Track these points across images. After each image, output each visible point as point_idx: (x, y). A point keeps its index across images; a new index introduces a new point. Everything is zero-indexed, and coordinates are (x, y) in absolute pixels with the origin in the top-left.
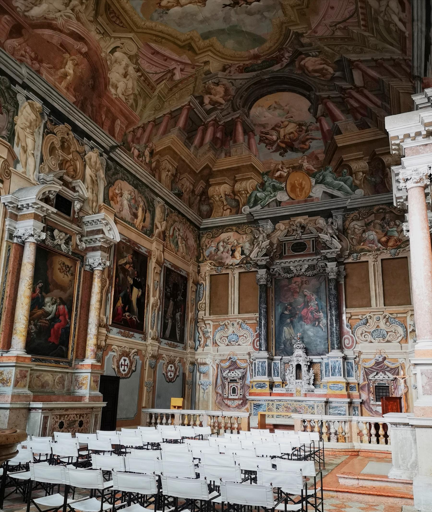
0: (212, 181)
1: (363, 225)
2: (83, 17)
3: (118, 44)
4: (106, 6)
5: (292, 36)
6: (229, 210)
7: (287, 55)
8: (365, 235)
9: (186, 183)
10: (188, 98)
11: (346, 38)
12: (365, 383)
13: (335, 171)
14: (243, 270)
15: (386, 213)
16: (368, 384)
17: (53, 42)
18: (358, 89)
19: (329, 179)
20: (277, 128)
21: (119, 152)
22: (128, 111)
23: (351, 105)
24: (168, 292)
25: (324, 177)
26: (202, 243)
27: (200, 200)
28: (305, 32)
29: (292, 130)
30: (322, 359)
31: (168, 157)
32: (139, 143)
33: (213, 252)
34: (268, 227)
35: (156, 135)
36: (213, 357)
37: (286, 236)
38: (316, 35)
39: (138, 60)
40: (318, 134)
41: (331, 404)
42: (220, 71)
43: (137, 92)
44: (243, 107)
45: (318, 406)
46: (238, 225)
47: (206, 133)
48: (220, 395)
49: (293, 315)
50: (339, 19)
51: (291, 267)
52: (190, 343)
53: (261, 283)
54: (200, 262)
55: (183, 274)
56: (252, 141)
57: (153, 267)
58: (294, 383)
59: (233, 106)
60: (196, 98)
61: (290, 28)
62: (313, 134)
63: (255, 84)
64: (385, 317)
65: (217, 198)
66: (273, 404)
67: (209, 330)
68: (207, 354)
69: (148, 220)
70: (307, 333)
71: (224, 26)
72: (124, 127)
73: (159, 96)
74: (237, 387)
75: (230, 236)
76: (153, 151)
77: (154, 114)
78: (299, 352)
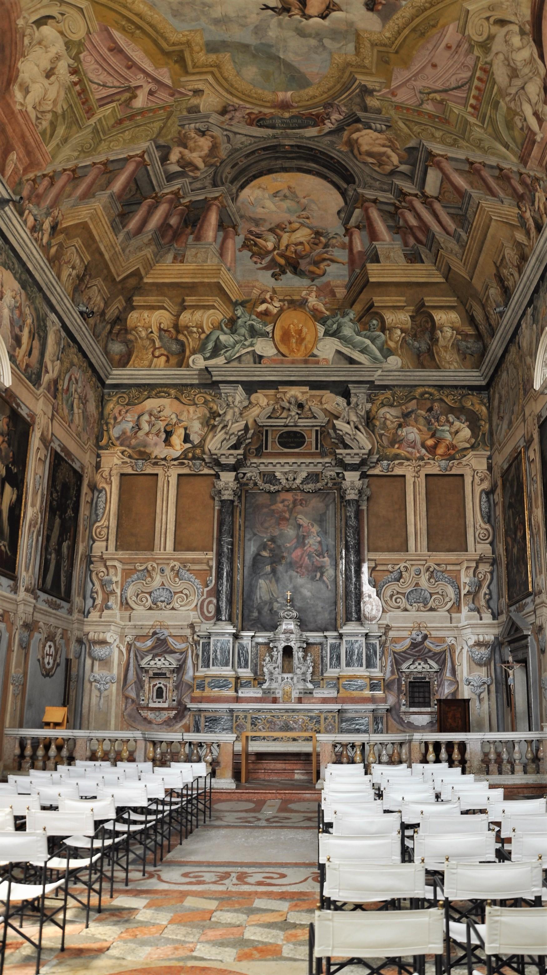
0: (138, 300)
1: (399, 414)
5: (355, 89)
6: (163, 359)
7: (335, 116)
8: (403, 432)
9: (96, 294)
10: (145, 145)
11: (438, 117)
12: (394, 677)
13: (360, 320)
14: (186, 471)
15: (433, 401)
16: (399, 680)
18: (426, 200)
19: (348, 331)
20: (278, 231)
21: (9, 213)
22: (36, 141)
23: (406, 221)
24: (53, 499)
26: (106, 412)
27: (110, 332)
28: (377, 88)
29: (302, 239)
30: (326, 637)
31: (78, 242)
32: (38, 205)
33: (128, 431)
34: (238, 398)
35: (69, 196)
36: (119, 630)
37: (270, 417)
38: (394, 99)
39: (81, 53)
40: (342, 255)
41: (344, 715)
43: (60, 111)
44: (232, 182)
45: (326, 719)
46: (182, 388)
47: (153, 213)
48: (133, 701)
49: (276, 559)
50: (438, 86)
51: (277, 474)
52: (77, 600)
53: (225, 497)
54: (101, 448)
55: (76, 466)
56: (230, 243)
57: (35, 448)
58: (280, 680)
60: (158, 147)
61: (356, 76)
62: (335, 254)
63: (264, 149)
64: (428, 570)
65: (143, 334)
66: (246, 717)
67: (114, 579)
68: (108, 624)
69: (36, 353)
70: (300, 593)
71: (251, 40)
72: (21, 169)
73: (95, 128)
74: (166, 686)
75: (167, 407)
76: (57, 224)
77: (77, 158)
78: (289, 625)
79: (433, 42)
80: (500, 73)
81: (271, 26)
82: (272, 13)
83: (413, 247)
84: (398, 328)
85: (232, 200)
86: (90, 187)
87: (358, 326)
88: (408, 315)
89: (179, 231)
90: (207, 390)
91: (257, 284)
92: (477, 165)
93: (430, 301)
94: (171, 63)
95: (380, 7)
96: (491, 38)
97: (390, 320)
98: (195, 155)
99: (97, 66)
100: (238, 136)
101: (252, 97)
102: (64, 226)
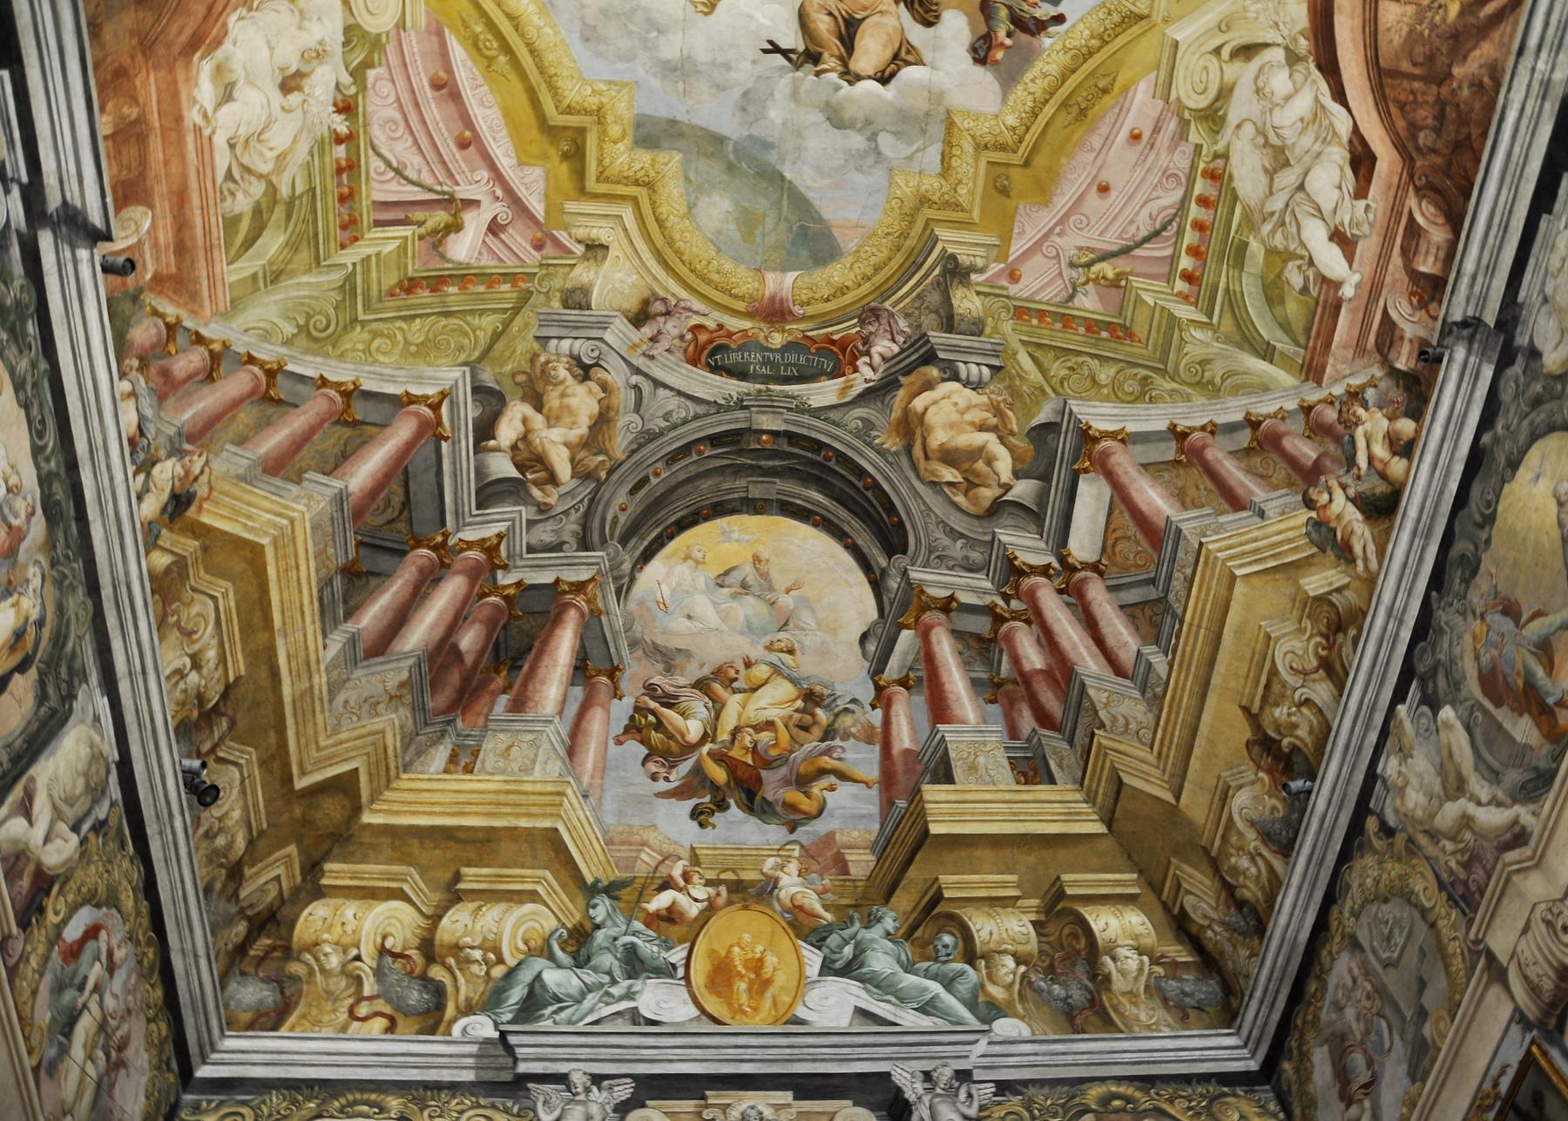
5: (932, 269)
7: (883, 347)
10: (447, 375)
11: (1109, 326)
13: (909, 935)
19: (881, 961)
20: (717, 687)
22: (207, 232)
23: (1016, 660)
25: (860, 951)
28: (980, 262)
29: (773, 714)
35: (241, 441)
39: (371, 66)
40: (863, 759)
42: (625, 314)
43: (284, 191)
44: (624, 540)
47: (426, 596)
50: (1111, 242)
59: (588, 515)
60: (478, 390)
62: (849, 756)
65: (334, 962)
71: (728, 125)
73: (350, 278)
77: (288, 342)
81: (777, 96)
82: (784, 62)
83: (1029, 740)
84: (1005, 952)
85: (618, 593)
87: (907, 951)
88: (1026, 919)
89: (478, 676)
90: (498, 1101)
91: (651, 837)
92: (1196, 435)
93: (1077, 882)
94: (553, 153)
95: (1000, 55)
96: (1225, 93)
97: (984, 934)
99: (397, 116)
100: (661, 392)
101: (708, 282)
102: (206, 519)
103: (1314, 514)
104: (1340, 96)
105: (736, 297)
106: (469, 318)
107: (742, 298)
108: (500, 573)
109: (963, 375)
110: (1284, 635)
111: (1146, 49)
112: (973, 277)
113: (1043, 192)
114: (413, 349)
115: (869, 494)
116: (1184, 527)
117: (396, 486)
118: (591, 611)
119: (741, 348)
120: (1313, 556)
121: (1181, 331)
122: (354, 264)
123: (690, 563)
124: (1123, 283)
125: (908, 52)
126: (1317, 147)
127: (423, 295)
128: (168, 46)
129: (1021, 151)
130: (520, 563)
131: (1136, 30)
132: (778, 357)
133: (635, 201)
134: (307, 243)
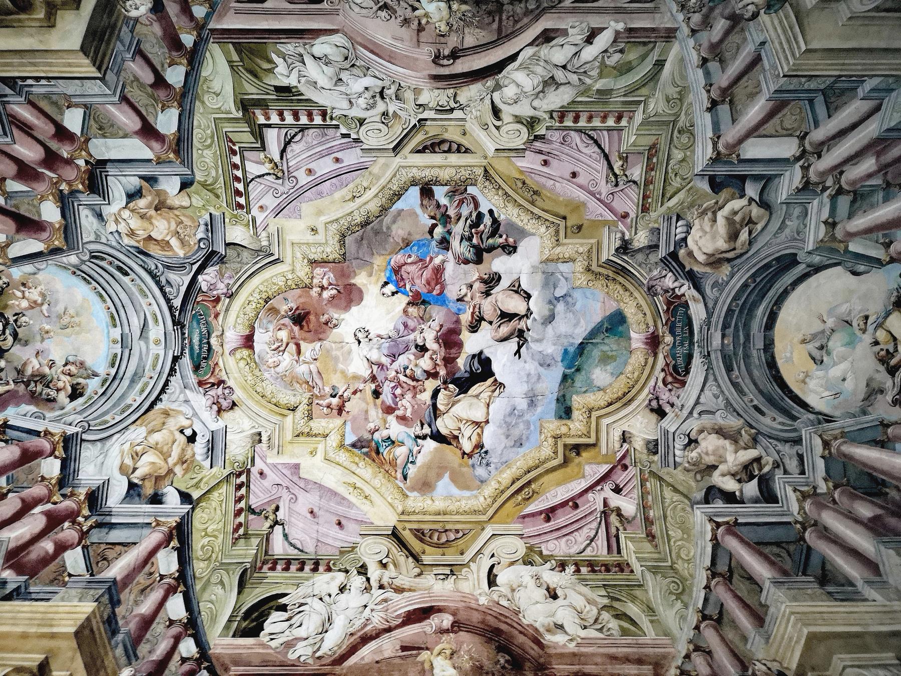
2: (403, 581)
3: (486, 563)
4: (416, 536)
7: (669, 282)
10: (699, 517)
17: (386, 656)
22: (629, 646)
23: (870, 176)
28: (619, 235)
35: (745, 639)
38: (632, 215)
39: (541, 552)
43: (606, 601)
44: (794, 418)
47: (836, 535)
50: (602, 166)
60: (707, 500)
61: (603, 260)
63: (729, 369)
71: (558, 371)
73: (649, 569)
77: (686, 606)
79: (543, 180)
80: (557, 99)
86: (746, 606)
89: (890, 506)
95: (511, 240)
96: (518, 120)
98: (730, 457)
99: (564, 539)
100: (702, 400)
101: (639, 378)
102: (794, 666)
103: (762, 11)
104: (513, 58)
105: (646, 363)
106: (667, 504)
107: (646, 359)
108: (819, 491)
109: (683, 235)
110: (849, 8)
111: (501, 165)
112: (627, 238)
113: (578, 207)
114: (685, 536)
115: (758, 280)
116: (772, 89)
117: (767, 550)
118: (842, 437)
119: (674, 358)
120: (791, 5)
121: (650, 117)
122: (641, 566)
123: (807, 380)
124: (625, 155)
125: (514, 286)
126: (542, 63)
127: (655, 529)
128: (540, 657)
129: (558, 222)
130: (812, 479)
131: (491, 172)
132: (678, 338)
133: (598, 418)
134: (634, 588)
